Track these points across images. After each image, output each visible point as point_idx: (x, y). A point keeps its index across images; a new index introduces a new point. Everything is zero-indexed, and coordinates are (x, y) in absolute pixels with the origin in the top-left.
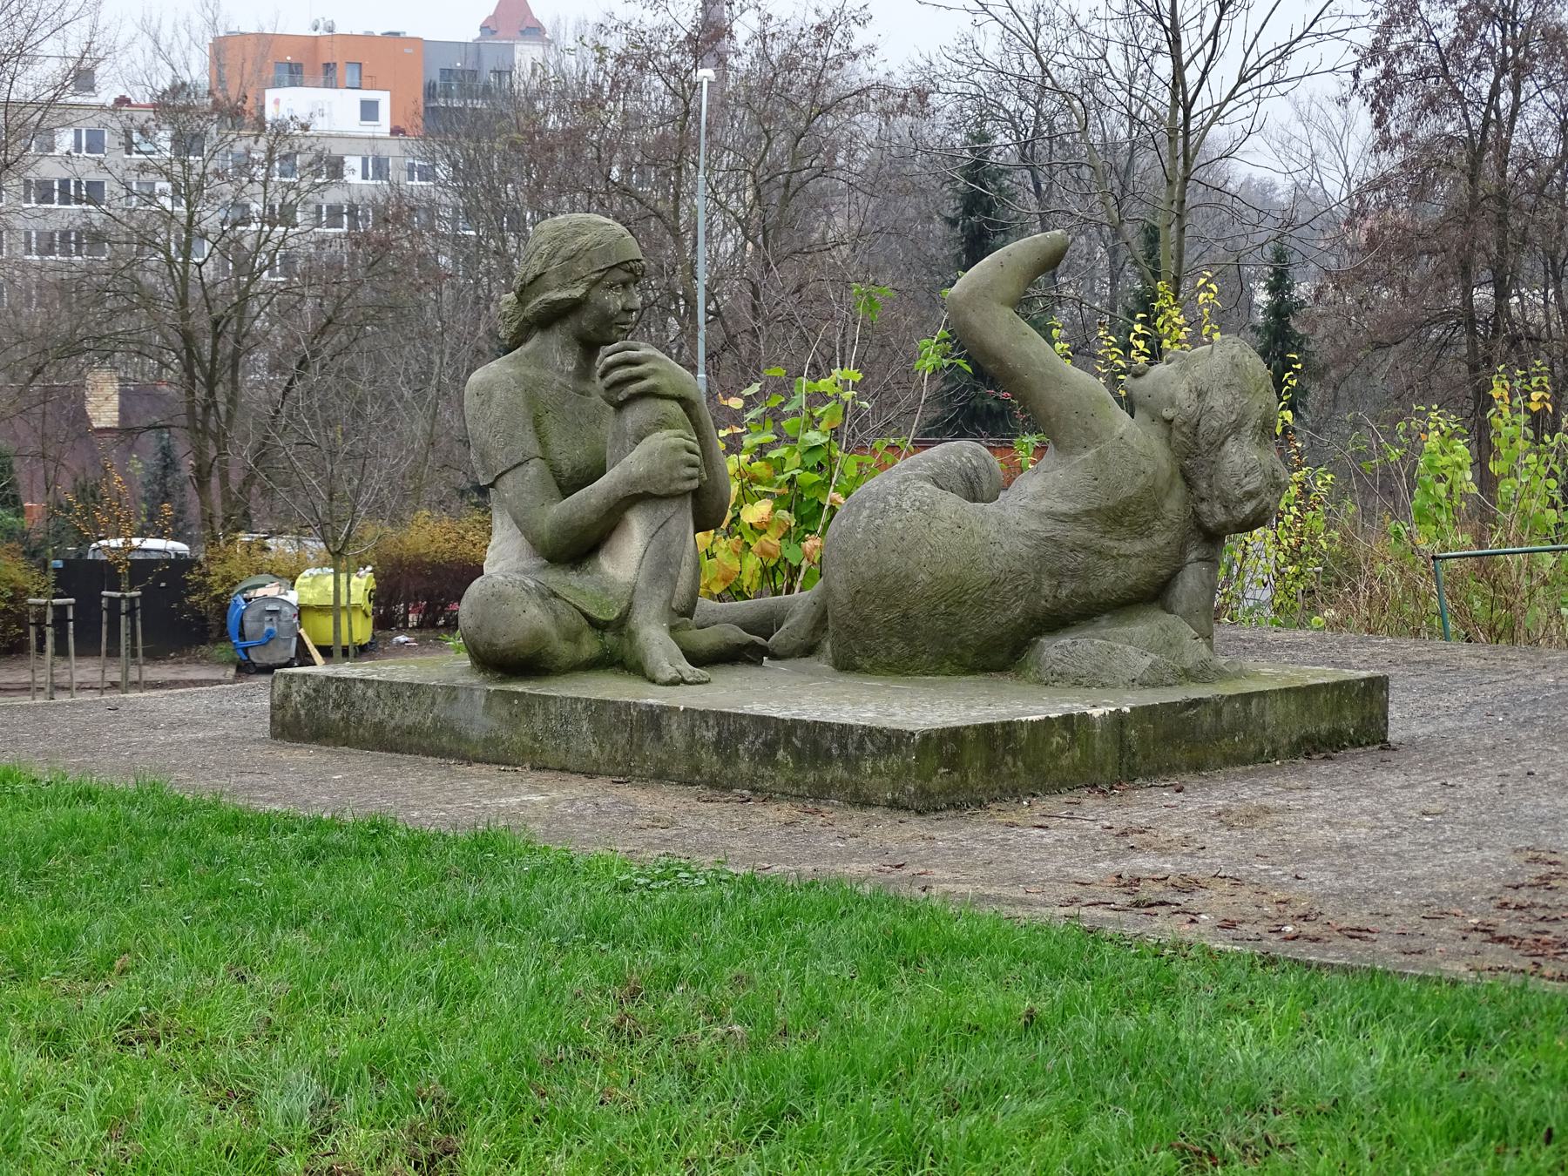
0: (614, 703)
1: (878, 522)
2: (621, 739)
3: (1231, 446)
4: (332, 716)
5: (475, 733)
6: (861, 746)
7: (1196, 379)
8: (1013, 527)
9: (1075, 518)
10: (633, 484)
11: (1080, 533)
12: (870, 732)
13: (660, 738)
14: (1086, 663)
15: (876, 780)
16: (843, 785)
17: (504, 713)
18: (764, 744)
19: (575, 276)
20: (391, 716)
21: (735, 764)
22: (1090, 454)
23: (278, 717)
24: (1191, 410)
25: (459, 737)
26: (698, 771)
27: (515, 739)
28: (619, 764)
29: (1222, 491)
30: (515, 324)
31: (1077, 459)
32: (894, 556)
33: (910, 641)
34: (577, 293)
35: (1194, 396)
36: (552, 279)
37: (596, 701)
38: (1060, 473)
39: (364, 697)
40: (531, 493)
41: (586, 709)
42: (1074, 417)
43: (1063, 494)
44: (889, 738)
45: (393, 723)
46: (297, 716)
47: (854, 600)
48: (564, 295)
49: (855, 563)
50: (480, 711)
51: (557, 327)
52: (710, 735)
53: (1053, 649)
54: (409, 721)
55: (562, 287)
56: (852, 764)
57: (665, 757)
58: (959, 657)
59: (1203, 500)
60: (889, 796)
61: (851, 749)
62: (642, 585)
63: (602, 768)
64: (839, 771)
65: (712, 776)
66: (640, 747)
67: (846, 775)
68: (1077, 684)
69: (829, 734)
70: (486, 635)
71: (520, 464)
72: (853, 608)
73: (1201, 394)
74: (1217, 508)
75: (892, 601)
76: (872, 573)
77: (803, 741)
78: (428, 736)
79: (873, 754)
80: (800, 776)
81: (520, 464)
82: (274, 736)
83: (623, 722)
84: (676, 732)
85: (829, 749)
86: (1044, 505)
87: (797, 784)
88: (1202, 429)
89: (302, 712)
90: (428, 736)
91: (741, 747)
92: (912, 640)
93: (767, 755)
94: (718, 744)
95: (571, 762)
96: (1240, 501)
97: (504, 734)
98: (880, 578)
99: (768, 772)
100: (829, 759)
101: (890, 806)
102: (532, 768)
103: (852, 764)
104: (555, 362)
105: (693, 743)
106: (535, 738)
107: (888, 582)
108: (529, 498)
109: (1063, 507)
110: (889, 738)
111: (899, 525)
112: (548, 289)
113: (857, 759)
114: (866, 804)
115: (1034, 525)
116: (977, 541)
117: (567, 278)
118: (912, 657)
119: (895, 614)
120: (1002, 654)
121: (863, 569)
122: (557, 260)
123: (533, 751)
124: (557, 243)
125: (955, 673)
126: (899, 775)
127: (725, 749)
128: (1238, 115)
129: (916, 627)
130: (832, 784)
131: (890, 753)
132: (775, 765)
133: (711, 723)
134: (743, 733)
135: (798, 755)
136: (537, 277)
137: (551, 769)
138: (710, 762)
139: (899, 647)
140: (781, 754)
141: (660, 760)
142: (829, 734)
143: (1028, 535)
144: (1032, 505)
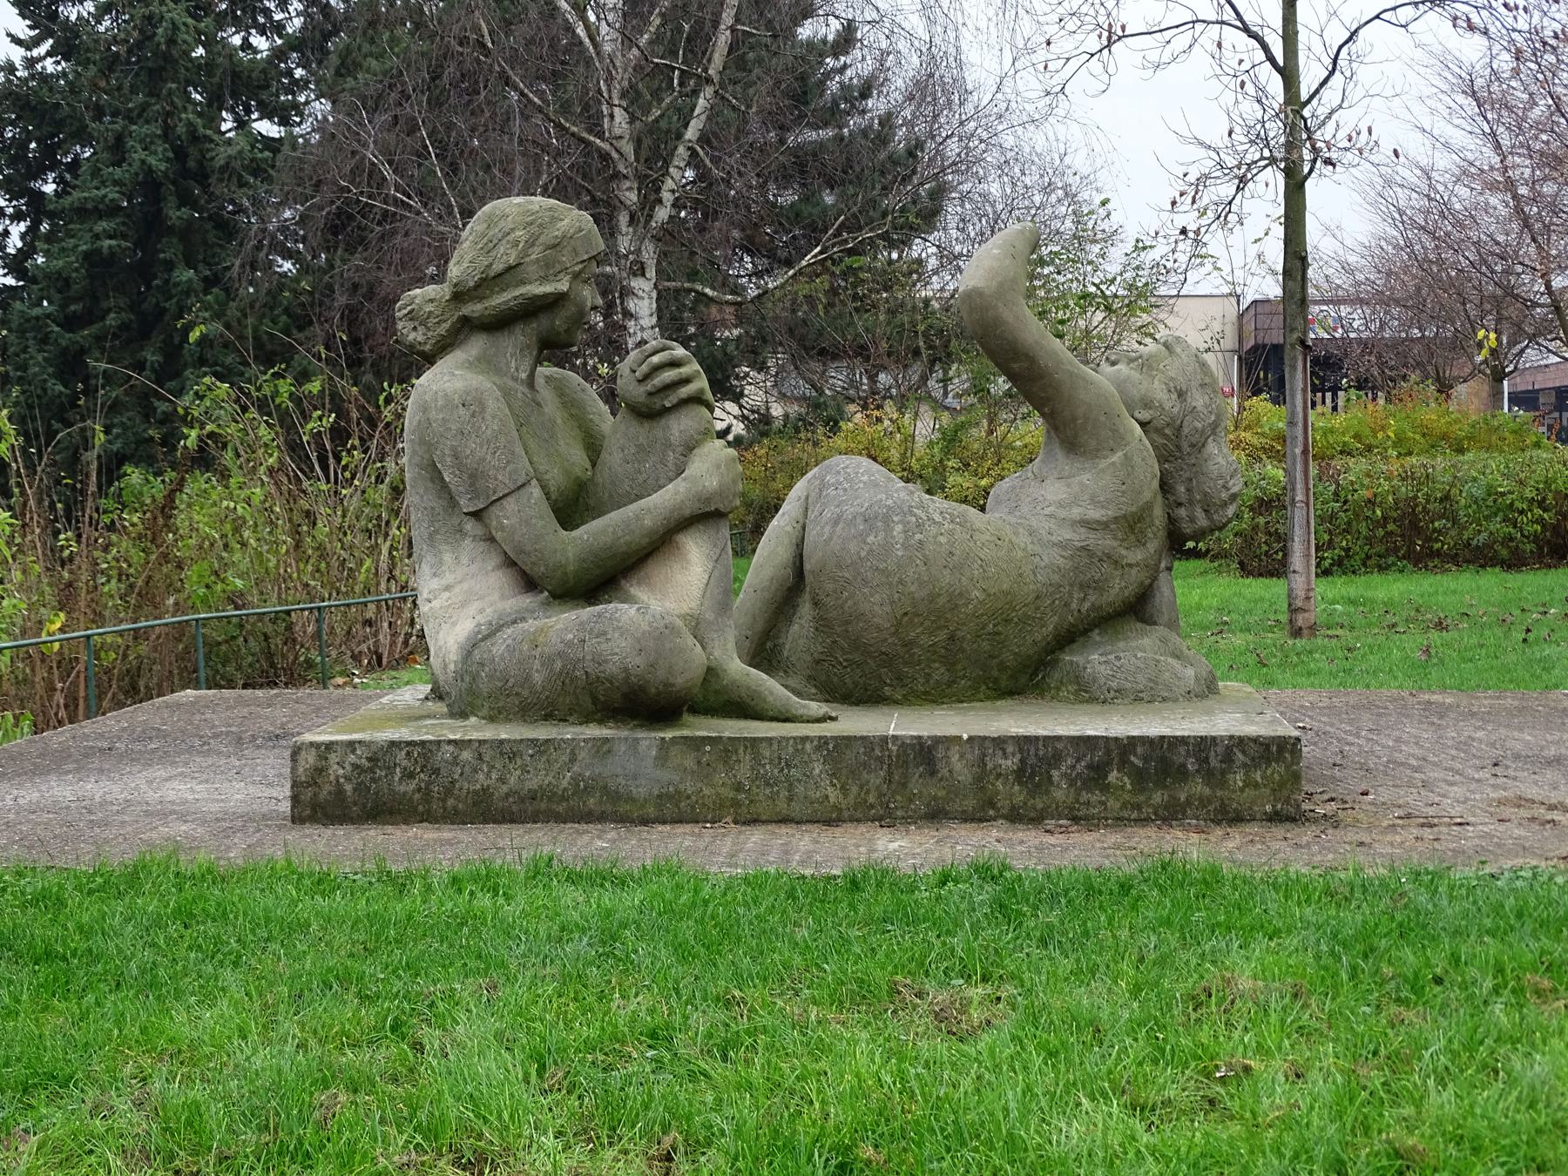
0: (863, 738)
1: (918, 536)
2: (875, 779)
3: (1212, 448)
4: (402, 788)
5: (641, 790)
6: (1228, 758)
7: (1172, 379)
8: (1046, 537)
9: (1104, 526)
10: (708, 500)
11: (1106, 542)
12: (1241, 742)
13: (933, 773)
14: (1140, 677)
15: (1250, 793)
16: (1204, 802)
17: (689, 762)
18: (1089, 767)
19: (558, 267)
20: (502, 780)
21: (1047, 792)
22: (1117, 457)
23: (307, 794)
24: (1175, 410)
25: (615, 797)
26: (992, 805)
27: (706, 791)
28: (872, 806)
29: (1205, 494)
30: (447, 325)
31: (1103, 464)
32: (946, 572)
33: (950, 665)
34: (563, 286)
35: (1174, 396)
36: (532, 271)
37: (834, 738)
38: (1086, 478)
39: (455, 761)
40: (541, 517)
41: (818, 749)
42: (1103, 419)
43: (1093, 500)
44: (1268, 746)
45: (505, 789)
46: (340, 792)
47: (900, 623)
48: (548, 288)
49: (901, 581)
50: (649, 762)
51: (518, 329)
52: (1010, 763)
53: (1095, 660)
54: (533, 783)
55: (544, 279)
56: (1215, 778)
57: (942, 793)
58: (996, 681)
59: (1180, 505)
60: (1268, 808)
61: (1214, 762)
62: (710, 616)
63: (846, 814)
64: (1199, 787)
65: (1013, 808)
66: (904, 785)
67: (1207, 791)
68: (1138, 699)
69: (1182, 750)
70: (661, 674)
71: (523, 485)
72: (896, 633)
73: (1181, 394)
74: (1199, 513)
75: (942, 622)
76: (924, 593)
77: (1145, 759)
78: (563, 798)
79: (1245, 765)
80: (1142, 798)
81: (523, 485)
82: (297, 819)
83: (878, 758)
84: (959, 767)
85: (1184, 765)
86: (1076, 512)
87: (1138, 807)
88: (1186, 430)
89: (348, 788)
90: (563, 798)
91: (1055, 773)
92: (954, 664)
93: (1096, 776)
94: (1020, 774)
95: (797, 809)
96: (1225, 505)
97: (689, 786)
98: (932, 598)
99: (1096, 797)
100: (1183, 774)
101: (1270, 820)
102: (736, 822)
103: (1215, 778)
104: (508, 367)
105: (982, 775)
106: (738, 787)
107: (942, 601)
108: (541, 523)
109: (1095, 514)
110: (1268, 746)
111: (943, 539)
112: (523, 283)
113: (1223, 773)
114: (1237, 819)
115: (1067, 534)
116: (1020, 554)
117: (549, 269)
118: (950, 684)
119: (942, 635)
120: (1029, 677)
121: (913, 589)
122: (537, 249)
123: (736, 804)
124: (534, 229)
125: (988, 698)
126: (1282, 784)
127: (1033, 774)
128: (1330, 96)
129: (962, 650)
130: (1188, 803)
131: (1268, 764)
132: (1105, 788)
133: (1010, 749)
134: (1056, 759)
135: (1139, 777)
136: (510, 269)
137: (764, 822)
138: (1009, 792)
139: (939, 673)
140: (1113, 777)
141: (935, 798)
142: (1182, 750)
143: (1062, 545)
144: (1063, 513)
